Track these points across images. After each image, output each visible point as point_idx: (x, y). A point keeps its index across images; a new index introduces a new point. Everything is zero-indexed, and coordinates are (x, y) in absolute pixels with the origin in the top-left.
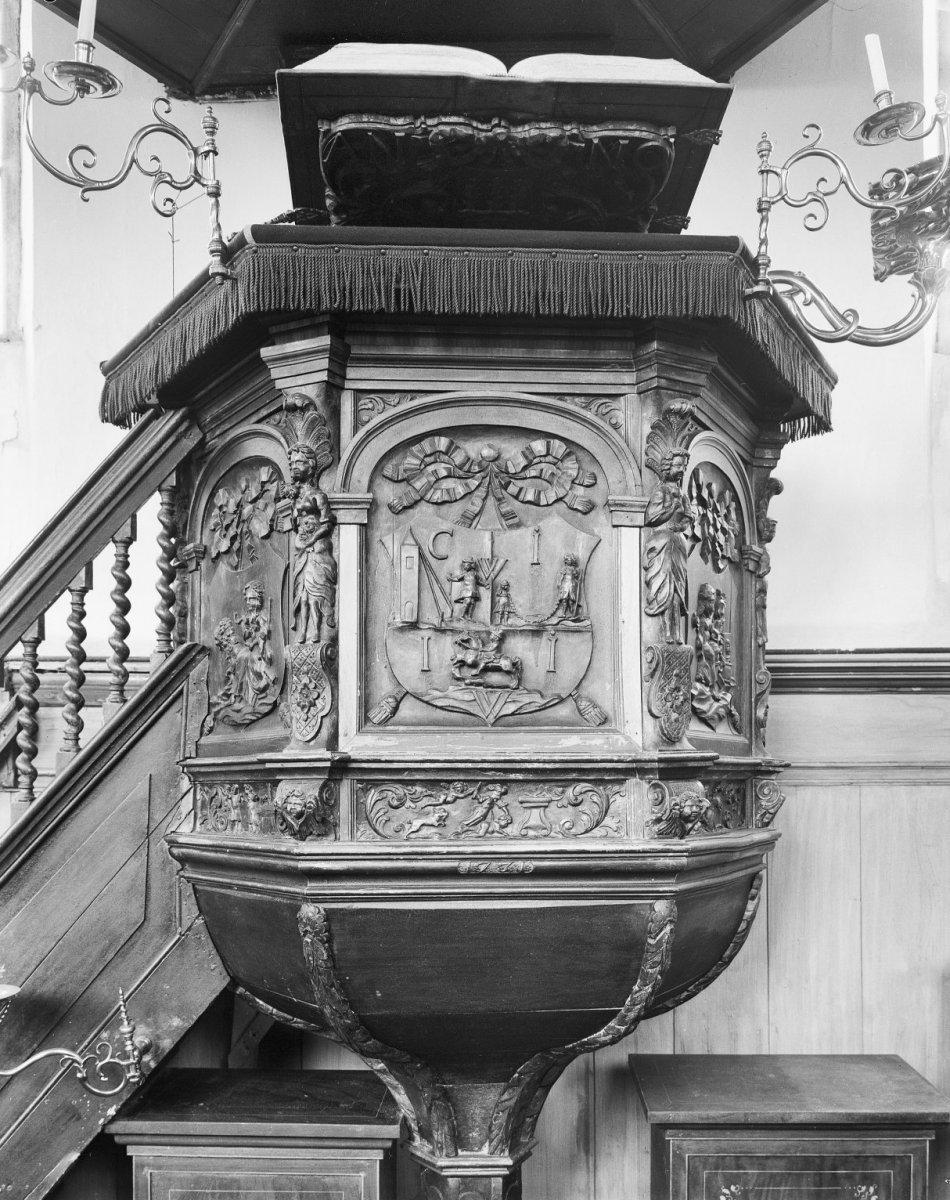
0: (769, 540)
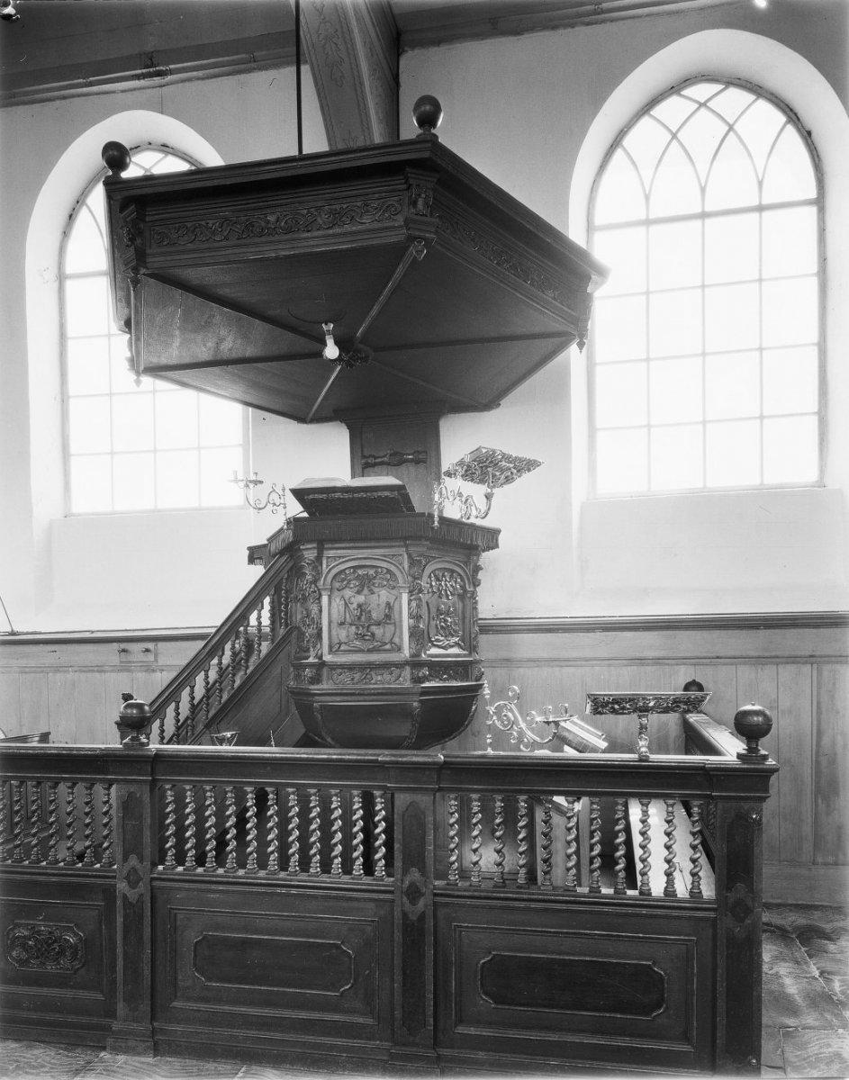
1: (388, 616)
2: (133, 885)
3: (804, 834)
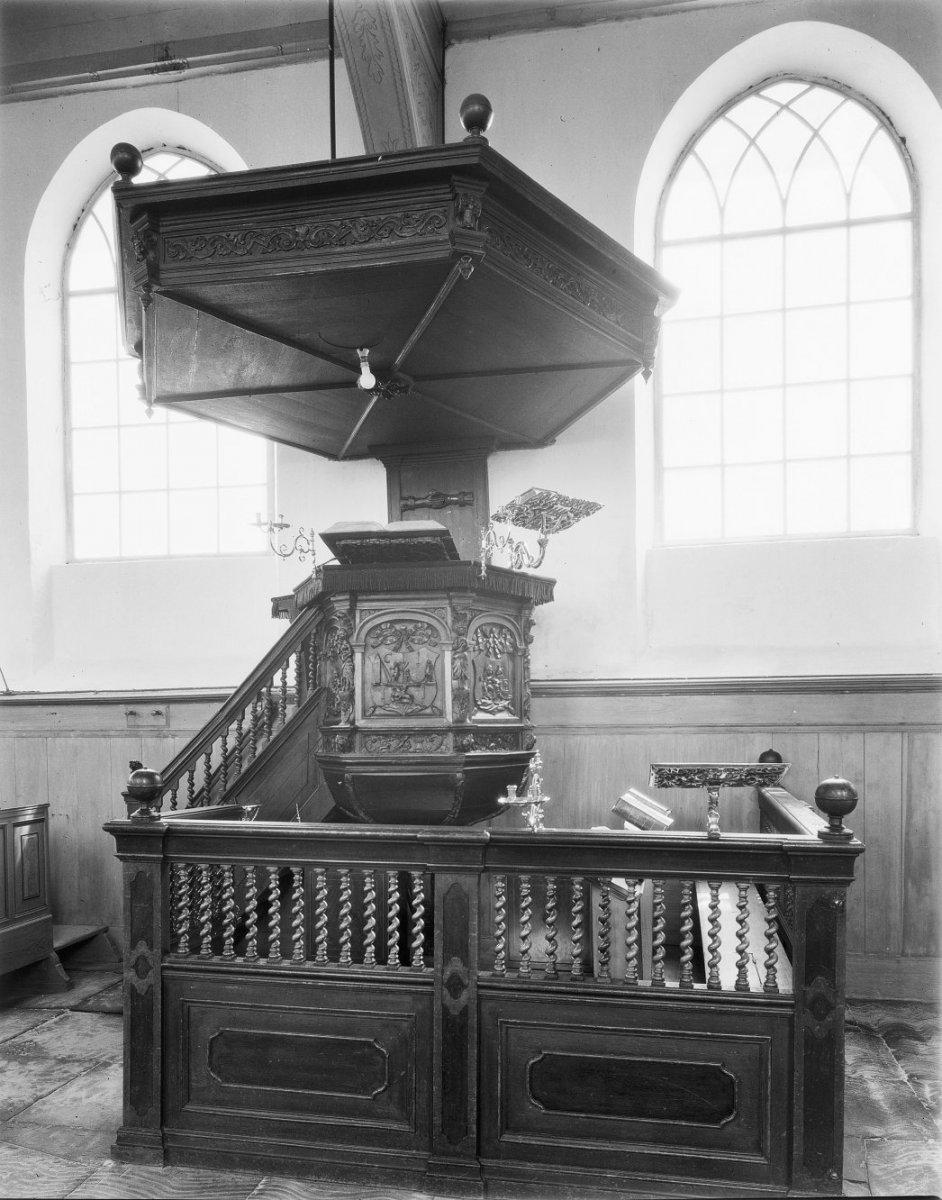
0: (530, 643)
1: (428, 677)
2: (141, 974)
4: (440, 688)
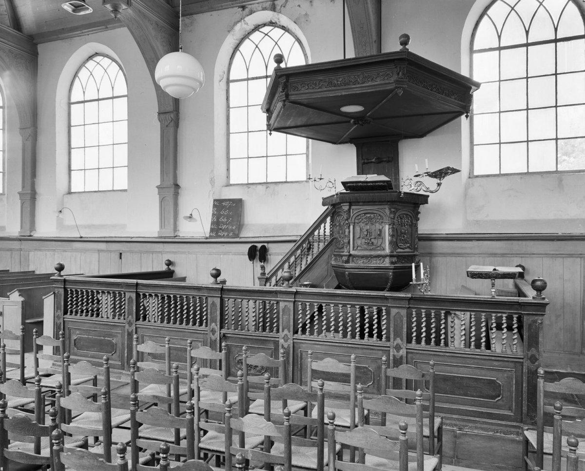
1: (379, 235)
2: (286, 341)
3: (576, 339)
4: (383, 239)
